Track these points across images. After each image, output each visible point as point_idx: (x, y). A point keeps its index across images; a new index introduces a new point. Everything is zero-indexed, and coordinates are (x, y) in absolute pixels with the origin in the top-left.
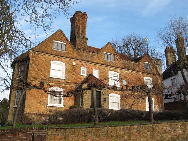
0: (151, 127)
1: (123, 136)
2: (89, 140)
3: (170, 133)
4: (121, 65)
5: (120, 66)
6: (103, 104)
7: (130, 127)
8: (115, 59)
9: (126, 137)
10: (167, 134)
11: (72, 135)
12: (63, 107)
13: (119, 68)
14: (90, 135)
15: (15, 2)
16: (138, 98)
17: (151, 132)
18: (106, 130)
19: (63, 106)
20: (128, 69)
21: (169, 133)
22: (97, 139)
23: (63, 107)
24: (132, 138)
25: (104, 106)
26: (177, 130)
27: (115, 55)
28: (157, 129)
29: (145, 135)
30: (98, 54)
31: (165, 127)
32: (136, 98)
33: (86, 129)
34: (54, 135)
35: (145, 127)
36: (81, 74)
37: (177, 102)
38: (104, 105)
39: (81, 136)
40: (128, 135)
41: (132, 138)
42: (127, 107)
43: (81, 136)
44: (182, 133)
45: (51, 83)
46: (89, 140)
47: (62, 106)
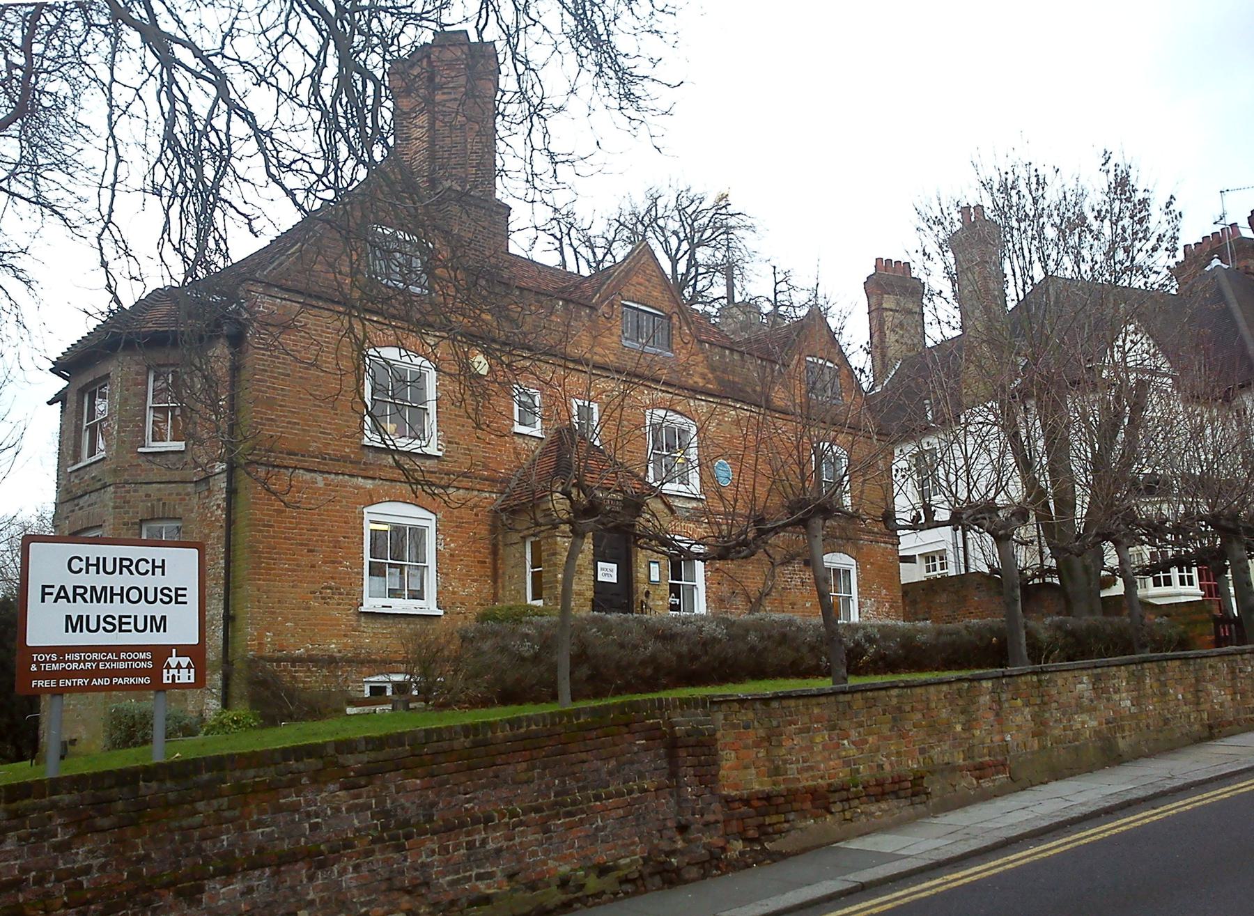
0: (1033, 687)
1: (949, 726)
2: (846, 742)
3: (1095, 709)
4: (703, 376)
5: (701, 383)
6: (647, 594)
7: (968, 688)
8: (677, 339)
9: (959, 728)
10: (1085, 717)
11: (790, 723)
12: (441, 613)
13: (695, 391)
14: (846, 724)
15: (1085, 276)
16: (787, 562)
17: (1036, 708)
18: (894, 701)
19: (438, 607)
20: (737, 401)
21: (1091, 710)
22: (870, 739)
23: (441, 613)
24: (977, 733)
25: (651, 603)
26: (1116, 697)
27: (675, 319)
28: (1054, 692)
29: (1019, 719)
30: (591, 308)
31: (1079, 686)
32: (778, 558)
33: (833, 698)
34: (734, 726)
35: (1017, 688)
36: (518, 428)
37: (946, 579)
38: (651, 596)
39: (818, 730)
40: (962, 718)
41: (977, 733)
42: (740, 614)
43: (818, 730)
44: (1133, 710)
45: (373, 479)
46: (846, 742)
47: (434, 610)
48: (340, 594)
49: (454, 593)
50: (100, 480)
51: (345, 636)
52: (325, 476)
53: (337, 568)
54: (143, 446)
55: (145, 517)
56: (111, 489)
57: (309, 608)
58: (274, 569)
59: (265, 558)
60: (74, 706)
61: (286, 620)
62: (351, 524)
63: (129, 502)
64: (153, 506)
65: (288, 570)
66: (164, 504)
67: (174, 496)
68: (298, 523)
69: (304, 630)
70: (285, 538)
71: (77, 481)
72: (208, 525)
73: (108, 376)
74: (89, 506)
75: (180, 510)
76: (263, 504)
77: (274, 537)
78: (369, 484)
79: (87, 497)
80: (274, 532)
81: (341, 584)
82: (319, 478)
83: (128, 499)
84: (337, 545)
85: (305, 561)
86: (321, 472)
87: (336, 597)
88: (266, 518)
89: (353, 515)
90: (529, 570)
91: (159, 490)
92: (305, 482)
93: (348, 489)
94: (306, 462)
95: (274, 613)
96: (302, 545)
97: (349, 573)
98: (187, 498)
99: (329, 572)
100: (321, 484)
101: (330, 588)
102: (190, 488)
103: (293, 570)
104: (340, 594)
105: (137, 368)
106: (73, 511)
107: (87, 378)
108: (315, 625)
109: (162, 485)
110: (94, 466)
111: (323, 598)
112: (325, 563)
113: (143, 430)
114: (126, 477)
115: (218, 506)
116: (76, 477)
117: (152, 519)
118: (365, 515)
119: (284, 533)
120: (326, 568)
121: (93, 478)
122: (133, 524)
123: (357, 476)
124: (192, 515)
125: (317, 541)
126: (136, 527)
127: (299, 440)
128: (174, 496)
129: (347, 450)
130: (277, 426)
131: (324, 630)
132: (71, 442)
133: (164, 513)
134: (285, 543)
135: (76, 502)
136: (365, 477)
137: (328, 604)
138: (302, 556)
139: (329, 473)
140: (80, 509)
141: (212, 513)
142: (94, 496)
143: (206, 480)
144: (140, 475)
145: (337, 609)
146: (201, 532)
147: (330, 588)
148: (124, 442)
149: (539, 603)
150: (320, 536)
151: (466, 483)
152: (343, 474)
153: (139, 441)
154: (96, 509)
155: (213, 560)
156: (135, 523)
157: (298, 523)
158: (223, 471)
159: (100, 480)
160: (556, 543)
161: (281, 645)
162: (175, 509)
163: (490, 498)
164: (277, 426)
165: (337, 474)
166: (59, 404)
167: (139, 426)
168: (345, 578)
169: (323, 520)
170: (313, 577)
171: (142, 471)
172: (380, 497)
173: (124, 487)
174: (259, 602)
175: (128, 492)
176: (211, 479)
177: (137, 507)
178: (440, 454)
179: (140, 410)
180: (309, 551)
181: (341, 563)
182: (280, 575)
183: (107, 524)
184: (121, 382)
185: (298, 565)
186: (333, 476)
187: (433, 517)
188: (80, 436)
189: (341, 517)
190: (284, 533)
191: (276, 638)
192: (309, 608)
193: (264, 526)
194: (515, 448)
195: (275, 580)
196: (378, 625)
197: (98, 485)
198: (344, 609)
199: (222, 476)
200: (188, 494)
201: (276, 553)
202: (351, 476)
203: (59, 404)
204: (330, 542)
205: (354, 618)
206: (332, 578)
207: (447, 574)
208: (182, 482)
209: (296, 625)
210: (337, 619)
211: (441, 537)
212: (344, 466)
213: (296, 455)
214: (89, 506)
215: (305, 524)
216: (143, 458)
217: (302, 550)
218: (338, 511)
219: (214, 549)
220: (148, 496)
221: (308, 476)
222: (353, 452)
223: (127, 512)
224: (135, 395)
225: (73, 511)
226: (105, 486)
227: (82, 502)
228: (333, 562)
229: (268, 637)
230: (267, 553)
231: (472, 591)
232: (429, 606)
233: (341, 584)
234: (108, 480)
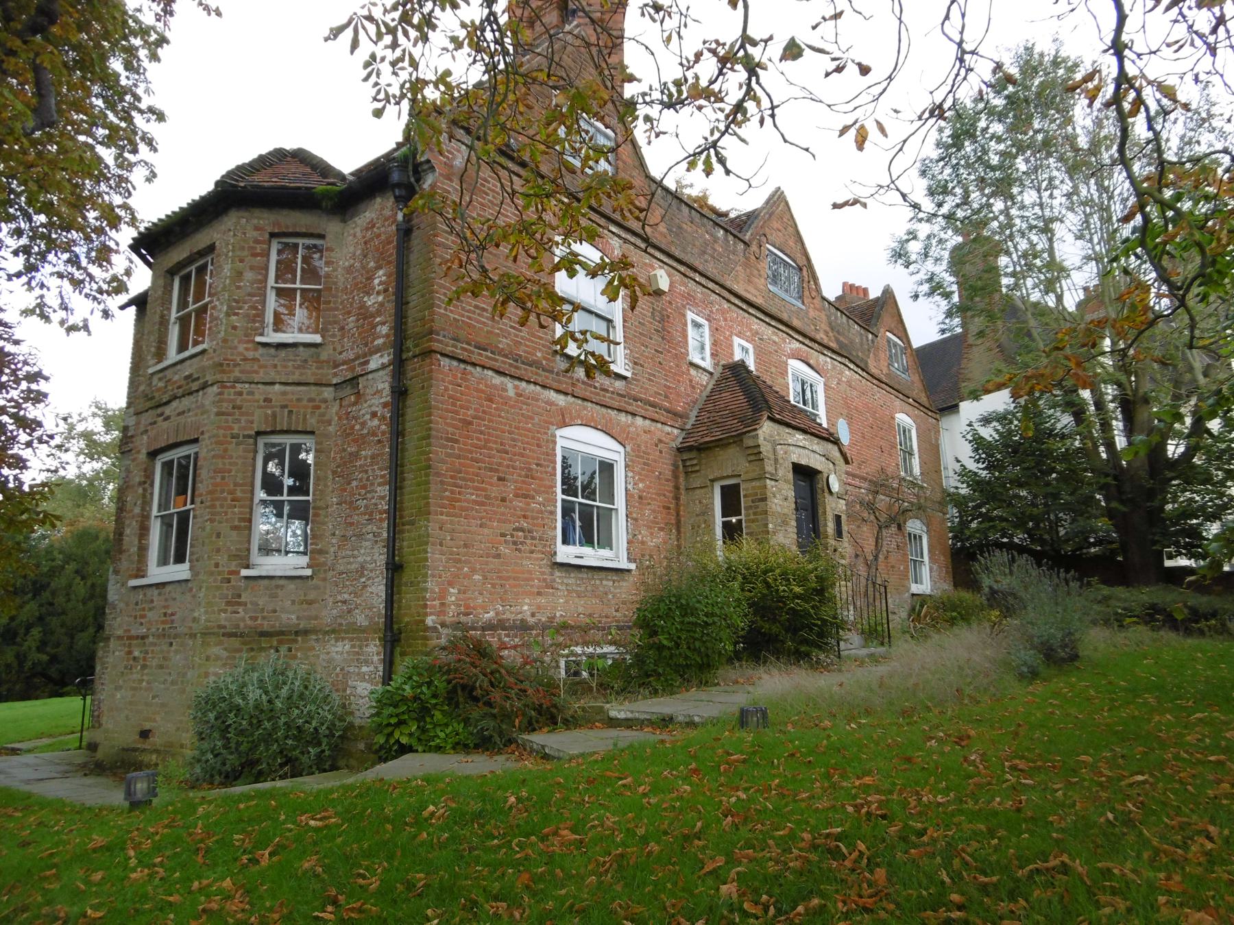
8: (807, 293)
12: (633, 566)
19: (630, 560)
23: (633, 566)
45: (566, 394)
47: (624, 564)
48: (533, 538)
49: (643, 543)
50: (198, 379)
51: (539, 594)
52: (517, 383)
53: (528, 504)
54: (262, 335)
55: (263, 428)
56: (215, 389)
57: (498, 556)
58: (459, 500)
59: (448, 484)
60: (148, 683)
61: (473, 571)
62: (544, 449)
63: (240, 408)
64: (274, 415)
65: (475, 502)
66: (290, 412)
67: (305, 402)
68: (487, 441)
69: (494, 586)
70: (473, 460)
71: (161, 384)
72: (355, 441)
73: (211, 248)
74: (179, 414)
75: (312, 422)
76: (447, 411)
77: (459, 457)
78: (561, 400)
79: (175, 404)
80: (460, 449)
81: (534, 525)
82: (510, 384)
83: (238, 403)
84: (530, 475)
85: (494, 491)
86: (512, 377)
87: (528, 541)
88: (450, 429)
89: (545, 437)
90: (719, 520)
91: (284, 393)
92: (495, 387)
93: (540, 403)
94: (496, 360)
95: (459, 561)
96: (491, 470)
97: (541, 512)
98: (323, 406)
99: (522, 509)
100: (511, 393)
101: (522, 530)
102: (328, 393)
103: (483, 504)
104: (533, 538)
105: (256, 234)
106: (155, 423)
107: (178, 254)
108: (508, 579)
109: (288, 388)
110: (188, 362)
111: (515, 543)
112: (516, 496)
113: (261, 315)
114: (237, 374)
115: (374, 415)
116: (160, 379)
117: (273, 432)
118: (558, 439)
119: (471, 452)
120: (519, 503)
121: (187, 378)
122: (245, 436)
123: (550, 388)
124: (331, 429)
125: (508, 467)
126: (251, 441)
127: (488, 332)
128: (305, 402)
129: (539, 354)
130: (463, 309)
131: (515, 586)
132: (153, 338)
133: (289, 423)
134: (472, 467)
135: (159, 411)
136: (558, 391)
137: (519, 550)
138: (491, 484)
139: (520, 379)
140: (166, 419)
141: (363, 424)
142: (186, 402)
143: (353, 381)
144: (257, 372)
145: (530, 558)
146: (344, 450)
147: (522, 530)
148: (235, 328)
149: (180, 571)
150: (511, 460)
151: (651, 412)
152: (535, 383)
153: (257, 329)
154: (190, 419)
155: (364, 487)
156: (249, 436)
157: (487, 441)
158: (384, 367)
159: (198, 379)
160: (765, 486)
161: (467, 606)
162: (305, 419)
163: (672, 434)
164: (463, 309)
165: (529, 382)
166: (133, 309)
167: (256, 308)
168: (537, 518)
169: (513, 440)
170: (503, 514)
171: (261, 367)
172: (572, 419)
173: (234, 387)
174: (441, 545)
175: (240, 394)
176: (360, 380)
177: (252, 414)
178: (628, 374)
179: (259, 288)
180: (500, 479)
181: (533, 498)
182: (467, 509)
183: (206, 436)
184: (233, 251)
185: (487, 497)
186: (524, 384)
187: (621, 449)
188: (167, 329)
189: (533, 438)
190: (471, 452)
191: (461, 596)
192: (498, 556)
193: (448, 440)
194: (691, 381)
195: (461, 516)
196: (572, 579)
197: (195, 386)
198: (537, 559)
199: (381, 373)
200: (325, 401)
201: (461, 479)
202: (544, 387)
203: (133, 309)
204: (521, 469)
205: (548, 570)
206: (525, 517)
207: (636, 520)
208: (316, 384)
209: (485, 578)
210: (530, 572)
211: (630, 474)
212: (537, 374)
213: (485, 350)
214: (179, 414)
215: (496, 442)
216: (261, 350)
217: (491, 477)
218: (529, 430)
219: (366, 472)
220: (267, 400)
221: (498, 380)
222: (545, 358)
223: (239, 421)
224: (252, 268)
225: (155, 423)
226: (204, 386)
227: (168, 410)
228: (526, 496)
229: (451, 594)
230: (452, 477)
231: (655, 540)
232: (616, 555)
233: (534, 525)
234: (210, 378)
